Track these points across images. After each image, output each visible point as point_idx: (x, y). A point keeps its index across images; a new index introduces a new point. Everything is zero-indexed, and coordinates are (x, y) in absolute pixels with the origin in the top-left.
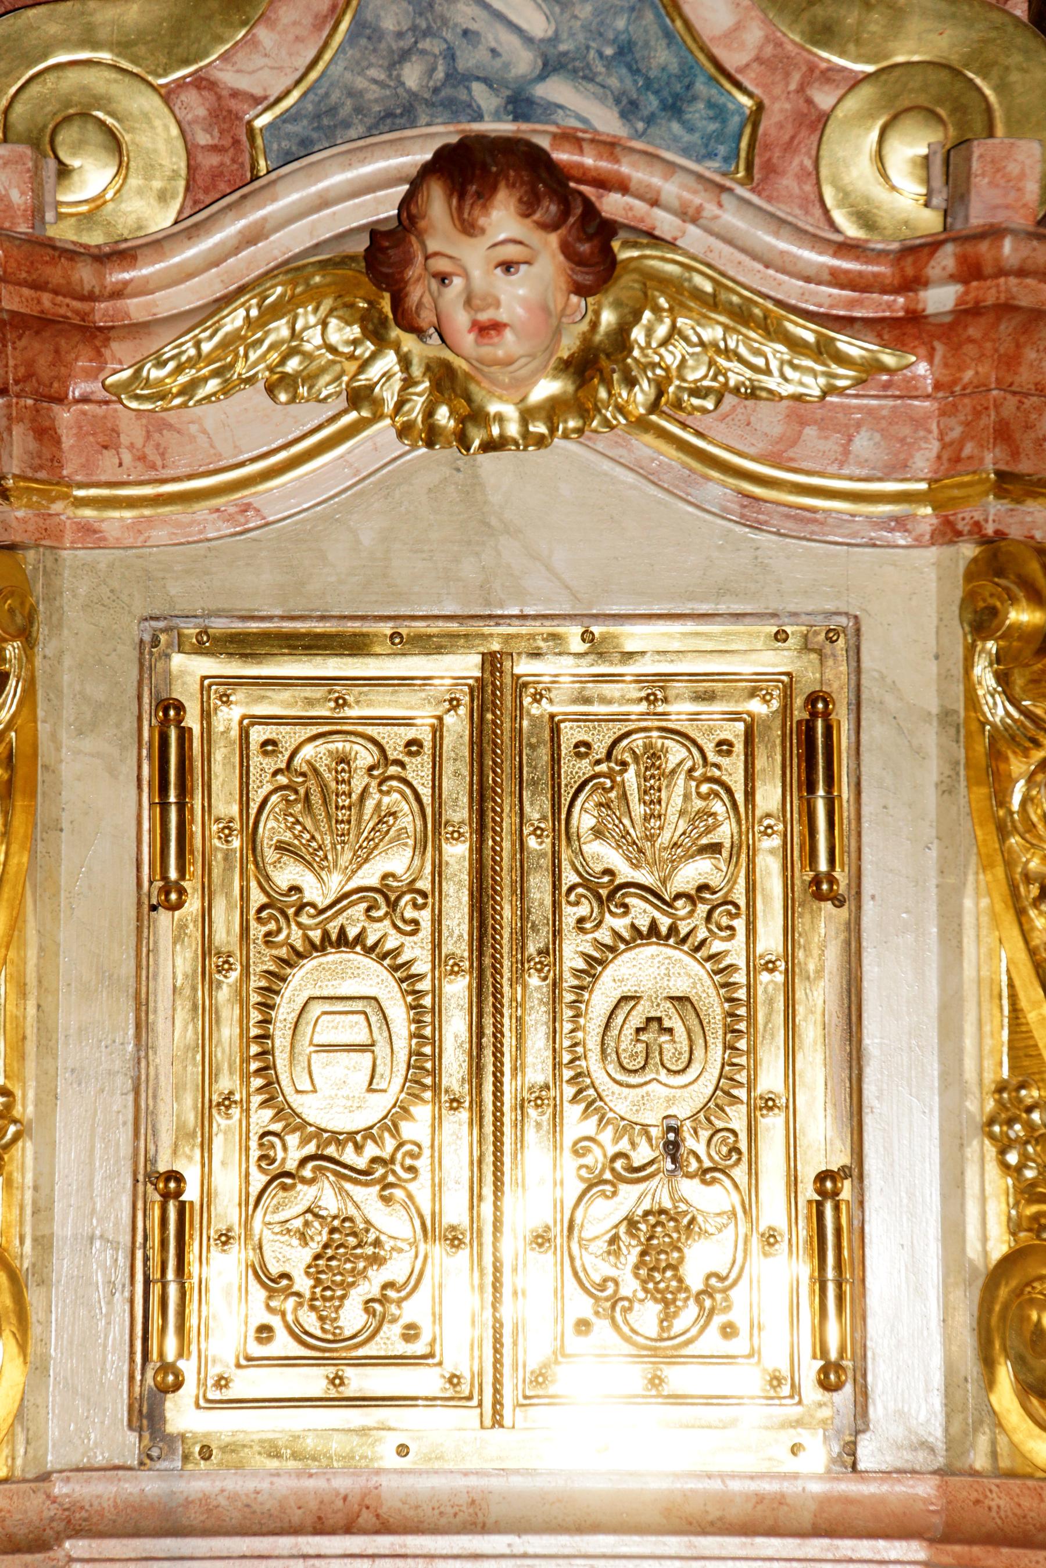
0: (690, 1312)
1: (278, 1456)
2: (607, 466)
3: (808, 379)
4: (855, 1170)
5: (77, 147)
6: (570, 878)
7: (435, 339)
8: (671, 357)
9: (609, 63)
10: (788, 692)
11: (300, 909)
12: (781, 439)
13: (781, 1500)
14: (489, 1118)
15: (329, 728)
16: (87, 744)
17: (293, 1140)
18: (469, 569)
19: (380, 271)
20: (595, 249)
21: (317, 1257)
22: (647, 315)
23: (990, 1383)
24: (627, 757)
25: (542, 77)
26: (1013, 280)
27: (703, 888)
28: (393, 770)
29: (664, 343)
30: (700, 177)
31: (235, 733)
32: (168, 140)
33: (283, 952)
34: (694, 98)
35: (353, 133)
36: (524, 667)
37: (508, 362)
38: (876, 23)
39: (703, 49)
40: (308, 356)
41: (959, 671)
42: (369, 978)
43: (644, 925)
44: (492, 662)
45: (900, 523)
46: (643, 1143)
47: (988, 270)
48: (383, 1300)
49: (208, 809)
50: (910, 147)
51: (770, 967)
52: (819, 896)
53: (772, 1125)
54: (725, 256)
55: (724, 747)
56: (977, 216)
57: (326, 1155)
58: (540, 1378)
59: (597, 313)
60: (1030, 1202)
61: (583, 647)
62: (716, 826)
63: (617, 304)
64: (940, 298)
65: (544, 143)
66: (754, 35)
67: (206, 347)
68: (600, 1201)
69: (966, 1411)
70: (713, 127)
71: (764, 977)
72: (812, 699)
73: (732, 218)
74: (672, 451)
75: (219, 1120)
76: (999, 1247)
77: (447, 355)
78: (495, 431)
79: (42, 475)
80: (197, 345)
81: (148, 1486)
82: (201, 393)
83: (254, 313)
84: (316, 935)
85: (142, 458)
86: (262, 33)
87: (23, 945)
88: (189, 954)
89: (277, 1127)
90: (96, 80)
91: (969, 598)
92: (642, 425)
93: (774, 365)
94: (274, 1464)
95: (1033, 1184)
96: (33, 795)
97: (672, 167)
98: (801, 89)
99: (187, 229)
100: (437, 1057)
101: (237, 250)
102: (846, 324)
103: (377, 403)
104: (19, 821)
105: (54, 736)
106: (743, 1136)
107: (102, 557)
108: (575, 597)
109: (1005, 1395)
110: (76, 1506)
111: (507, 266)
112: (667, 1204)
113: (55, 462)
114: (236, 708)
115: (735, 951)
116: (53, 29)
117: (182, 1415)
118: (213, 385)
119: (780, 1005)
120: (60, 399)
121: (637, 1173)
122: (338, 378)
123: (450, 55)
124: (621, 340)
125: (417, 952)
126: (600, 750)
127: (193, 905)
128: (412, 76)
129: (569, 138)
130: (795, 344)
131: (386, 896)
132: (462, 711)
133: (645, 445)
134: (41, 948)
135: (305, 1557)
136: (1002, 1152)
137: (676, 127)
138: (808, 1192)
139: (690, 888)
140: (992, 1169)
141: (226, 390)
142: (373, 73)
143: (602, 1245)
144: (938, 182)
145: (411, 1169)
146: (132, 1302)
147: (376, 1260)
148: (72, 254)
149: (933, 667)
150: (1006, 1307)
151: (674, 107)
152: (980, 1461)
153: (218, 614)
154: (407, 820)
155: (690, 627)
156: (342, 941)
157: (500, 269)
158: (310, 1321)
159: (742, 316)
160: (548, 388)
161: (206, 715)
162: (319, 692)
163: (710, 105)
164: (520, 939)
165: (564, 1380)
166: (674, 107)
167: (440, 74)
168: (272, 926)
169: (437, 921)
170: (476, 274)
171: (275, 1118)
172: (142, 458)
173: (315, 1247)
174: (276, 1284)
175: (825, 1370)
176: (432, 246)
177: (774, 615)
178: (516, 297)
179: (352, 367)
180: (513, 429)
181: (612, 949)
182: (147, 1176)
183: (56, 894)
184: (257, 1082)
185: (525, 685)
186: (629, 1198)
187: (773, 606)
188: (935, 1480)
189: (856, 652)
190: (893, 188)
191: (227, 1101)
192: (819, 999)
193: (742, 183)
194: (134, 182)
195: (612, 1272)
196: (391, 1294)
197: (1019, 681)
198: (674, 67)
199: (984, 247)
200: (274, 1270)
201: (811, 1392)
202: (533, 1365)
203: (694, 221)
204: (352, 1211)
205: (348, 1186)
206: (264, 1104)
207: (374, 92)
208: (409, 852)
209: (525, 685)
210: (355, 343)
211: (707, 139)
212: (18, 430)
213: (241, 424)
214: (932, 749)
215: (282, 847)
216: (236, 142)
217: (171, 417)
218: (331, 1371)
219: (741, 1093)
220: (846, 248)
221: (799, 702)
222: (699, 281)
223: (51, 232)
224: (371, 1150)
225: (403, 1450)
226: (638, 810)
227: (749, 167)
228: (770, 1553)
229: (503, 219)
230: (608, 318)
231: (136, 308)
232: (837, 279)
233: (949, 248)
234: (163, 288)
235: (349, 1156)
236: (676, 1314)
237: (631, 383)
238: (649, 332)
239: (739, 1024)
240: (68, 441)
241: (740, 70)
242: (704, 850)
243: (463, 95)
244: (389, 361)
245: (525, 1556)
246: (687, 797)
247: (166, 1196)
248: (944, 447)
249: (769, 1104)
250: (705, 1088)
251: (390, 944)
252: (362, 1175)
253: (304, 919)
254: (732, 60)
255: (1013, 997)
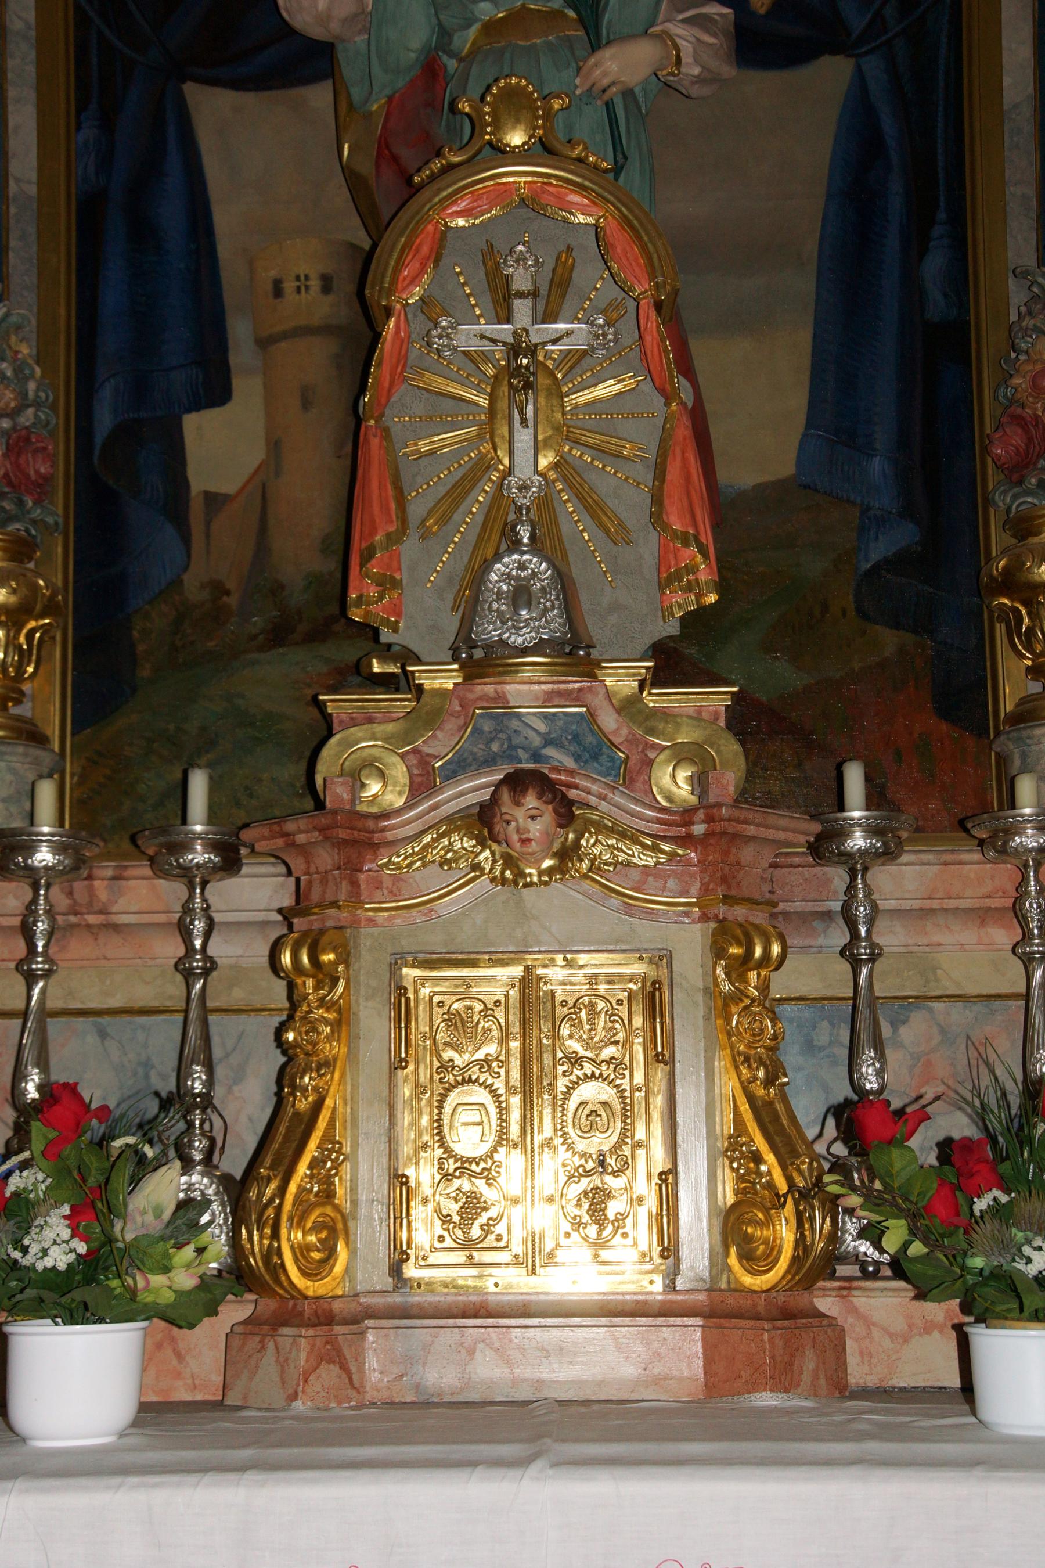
0: (610, 1228)
1: (447, 1287)
2: (572, 892)
3: (649, 859)
4: (674, 1171)
5: (368, 777)
6: (560, 1055)
7: (505, 845)
8: (596, 851)
9: (570, 742)
10: (644, 980)
11: (453, 1068)
12: (639, 881)
13: (646, 1302)
14: (529, 1151)
15: (466, 996)
16: (370, 1004)
17: (451, 1161)
18: (519, 933)
19: (483, 821)
20: (566, 811)
21: (461, 1208)
22: (587, 835)
23: (727, 1254)
24: (582, 1006)
25: (544, 747)
26: (726, 823)
27: (613, 1058)
28: (489, 1012)
29: (594, 845)
30: (606, 783)
31: (427, 999)
32: (403, 772)
33: (447, 1085)
34: (602, 754)
35: (472, 768)
36: (540, 971)
37: (533, 854)
38: (670, 728)
39: (605, 736)
40: (455, 852)
41: (710, 972)
42: (482, 1096)
43: (589, 1073)
44: (528, 969)
45: (686, 914)
46: (590, 1161)
47: (717, 819)
48: (488, 1225)
49: (417, 1029)
50: (683, 774)
51: (639, 1090)
52: (658, 1061)
53: (641, 1153)
54: (617, 813)
55: (620, 1002)
56: (712, 799)
57: (465, 1165)
58: (551, 1255)
59: (567, 835)
60: (742, 1182)
61: (564, 963)
62: (617, 1033)
63: (575, 831)
64: (699, 829)
65: (546, 771)
66: (624, 731)
67: (416, 849)
68: (573, 1184)
69: (718, 1263)
70: (609, 764)
71: (637, 1094)
72: (654, 983)
73: (618, 799)
74: (597, 887)
75: (422, 1154)
76: (730, 1200)
77: (509, 851)
78: (528, 880)
79: (353, 900)
80: (413, 849)
81: (397, 1299)
82: (414, 867)
83: (435, 836)
84: (459, 1078)
85: (391, 892)
86: (438, 733)
87: (345, 1084)
88: (410, 1086)
89: (445, 1156)
90: (375, 752)
91: (714, 943)
92: (585, 876)
93: (636, 854)
94: (446, 1290)
95: (743, 1175)
96: (348, 1024)
97: (595, 780)
98: (643, 751)
99: (408, 806)
100: (508, 1128)
101: (429, 813)
102: (663, 838)
103: (483, 869)
104: (343, 1034)
105: (357, 1001)
106: (629, 1158)
107: (375, 931)
108: (560, 944)
109: (733, 1260)
110: (369, 1307)
111: (533, 818)
112: (600, 1186)
113: (358, 894)
114: (424, 986)
115: (626, 1084)
116: (360, 734)
117: (410, 1271)
118: (418, 864)
119: (643, 1105)
120: (361, 871)
121: (588, 1173)
122: (467, 860)
123: (509, 739)
124: (577, 844)
125: (499, 1085)
126: (571, 1003)
127: (411, 1067)
128: (495, 747)
129: (555, 769)
130: (644, 846)
131: (486, 1063)
132: (516, 988)
133: (586, 885)
134: (352, 1085)
135: (459, 1327)
136: (731, 1163)
137: (596, 764)
138: (656, 1180)
139: (607, 1058)
140: (727, 1170)
141: (424, 865)
142: (480, 746)
143: (575, 1202)
144: (696, 786)
145: (498, 1172)
146: (389, 1226)
147: (485, 1209)
148: (366, 816)
149: (700, 970)
150: (733, 1224)
151: (595, 757)
152: (724, 1286)
153: (420, 952)
154: (495, 1033)
155: (606, 955)
156: (470, 1080)
157: (530, 819)
158: (459, 1233)
159: (623, 835)
160: (547, 863)
161: (416, 992)
162: (459, 982)
163: (609, 756)
164: (540, 1080)
165: (561, 1255)
166: (595, 757)
167: (506, 746)
168: (442, 1075)
169: (507, 1073)
170: (521, 820)
171: (444, 1152)
172: (391, 892)
173: (460, 1204)
174: (446, 1219)
175: (663, 1251)
176: (504, 810)
177: (638, 950)
178: (535, 829)
179: (473, 856)
180: (535, 879)
181: (577, 1083)
182: (394, 1175)
183: (358, 1063)
184: (437, 1138)
185: (541, 978)
186: (585, 1183)
187: (638, 946)
188: (706, 1293)
189: (670, 965)
190: (679, 787)
191: (425, 1146)
192: (658, 1102)
193: (621, 785)
194: (389, 788)
195: (578, 1213)
196: (491, 1222)
197: (734, 976)
198: (595, 742)
199: (715, 811)
200: (445, 1213)
201: (658, 1260)
202: (548, 1250)
203: (604, 800)
204: (475, 1189)
205: (473, 1179)
206: (439, 1147)
207: (481, 753)
208: (495, 1045)
209: (541, 978)
210: (474, 846)
211: (608, 769)
212: (344, 883)
213: (430, 880)
214: (701, 1004)
215: (446, 1044)
216: (428, 772)
217: (403, 876)
218: (468, 1253)
219: (628, 1140)
220: (663, 810)
221: (648, 984)
222: (606, 821)
223: (358, 808)
224: (482, 1165)
225: (496, 1285)
226: (587, 1027)
227: (624, 780)
228: (641, 1323)
229: (531, 801)
230: (571, 836)
231: (389, 835)
232: (659, 821)
233: (702, 811)
234: (398, 828)
235: (474, 1167)
236: (604, 1229)
237: (581, 861)
238: (588, 841)
239: (627, 1113)
240: (363, 886)
241: (620, 744)
242: (612, 1043)
243: (513, 753)
244: (487, 853)
245: (545, 1326)
246: (605, 1022)
247: (402, 1184)
248: (702, 885)
249: (639, 1145)
250: (614, 1138)
251: (489, 1082)
252: (478, 1175)
253: (455, 1073)
254: (616, 740)
255: (735, 1101)
